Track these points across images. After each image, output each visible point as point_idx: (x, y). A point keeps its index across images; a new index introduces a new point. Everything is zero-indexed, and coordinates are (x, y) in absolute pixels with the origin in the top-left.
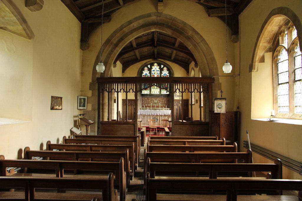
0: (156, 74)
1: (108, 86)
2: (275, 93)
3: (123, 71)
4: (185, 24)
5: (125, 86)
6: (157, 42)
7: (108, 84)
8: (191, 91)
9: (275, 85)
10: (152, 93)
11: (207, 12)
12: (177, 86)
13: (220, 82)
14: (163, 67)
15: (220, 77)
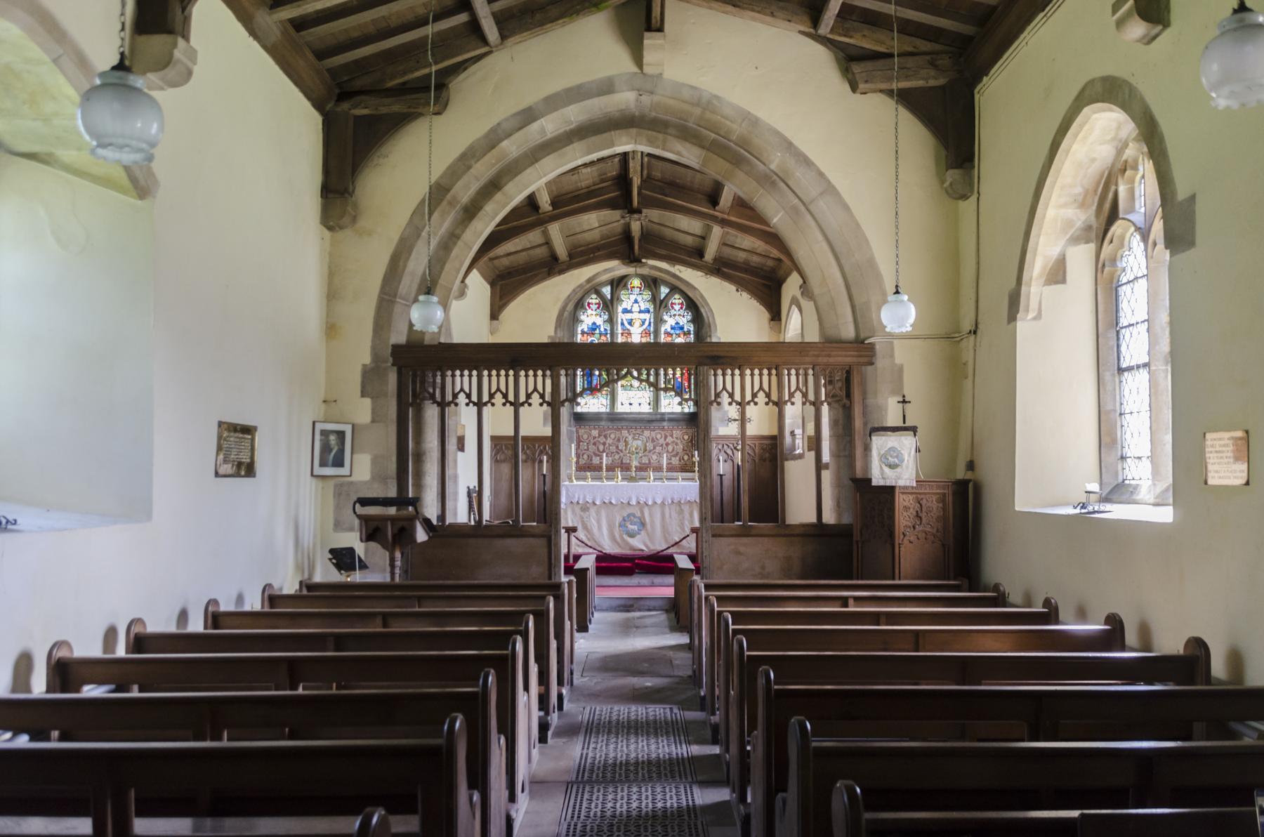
0: (637, 323)
1: (439, 379)
4: (755, 122)
6: (640, 189)
7: (439, 373)
9: (1107, 376)
10: (620, 409)
11: (846, 72)
13: (898, 361)
15: (896, 342)
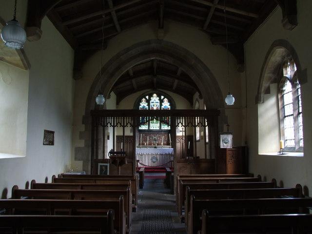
2: (282, 126)
3: (118, 103)
12: (179, 120)
14: (164, 99)
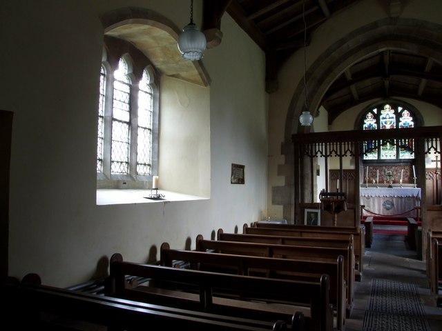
1: (310, 147)
3: (330, 122)
5: (338, 146)
8: (312, 154)
10: (382, 158)
